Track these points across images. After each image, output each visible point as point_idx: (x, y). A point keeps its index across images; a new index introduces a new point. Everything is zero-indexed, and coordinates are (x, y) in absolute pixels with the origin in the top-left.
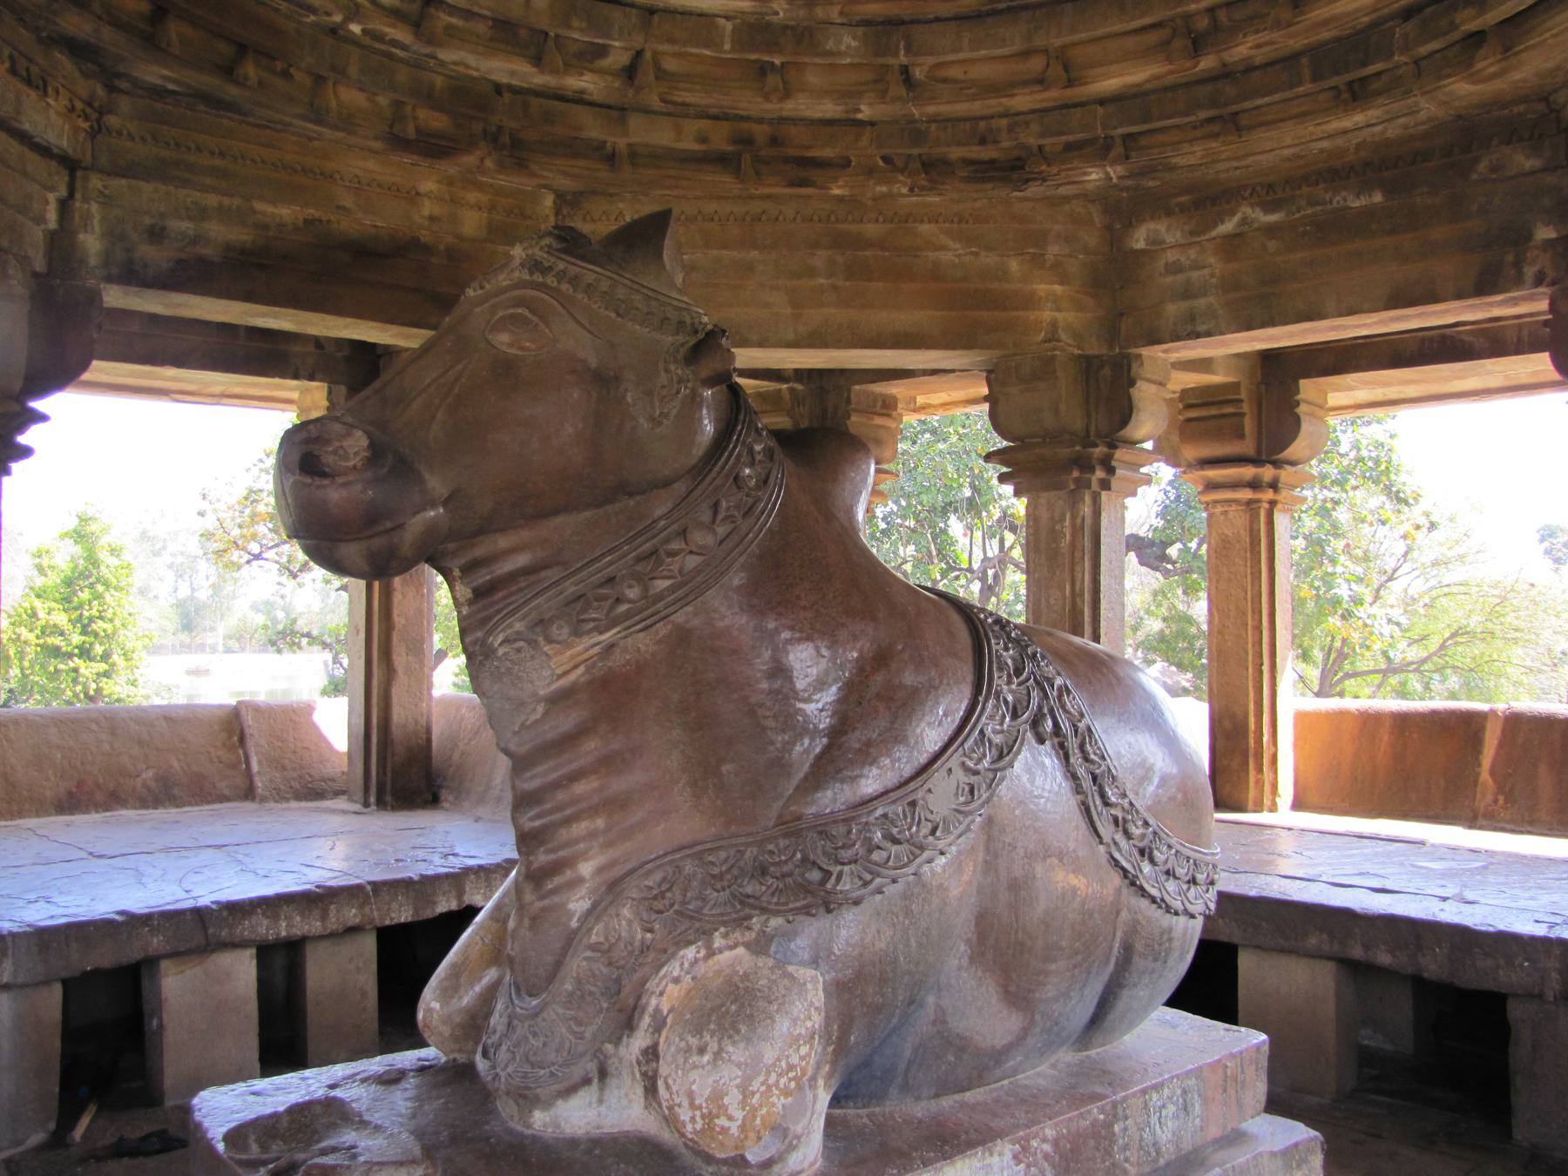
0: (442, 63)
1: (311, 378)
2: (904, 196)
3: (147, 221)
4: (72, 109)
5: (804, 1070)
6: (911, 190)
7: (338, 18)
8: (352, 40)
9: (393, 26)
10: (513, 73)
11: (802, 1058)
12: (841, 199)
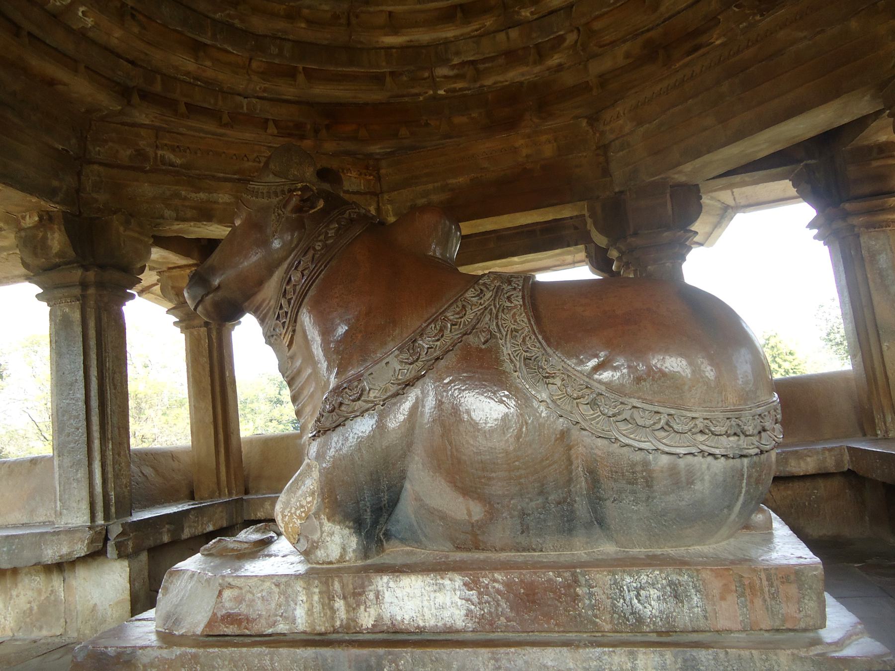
0: (489, 86)
1: (576, 244)
2: (760, 21)
3: (409, 204)
4: (361, 174)
5: (309, 510)
6: (762, 15)
7: (431, 92)
8: (442, 97)
9: (455, 83)
10: (523, 75)
11: (308, 503)
12: (722, 44)
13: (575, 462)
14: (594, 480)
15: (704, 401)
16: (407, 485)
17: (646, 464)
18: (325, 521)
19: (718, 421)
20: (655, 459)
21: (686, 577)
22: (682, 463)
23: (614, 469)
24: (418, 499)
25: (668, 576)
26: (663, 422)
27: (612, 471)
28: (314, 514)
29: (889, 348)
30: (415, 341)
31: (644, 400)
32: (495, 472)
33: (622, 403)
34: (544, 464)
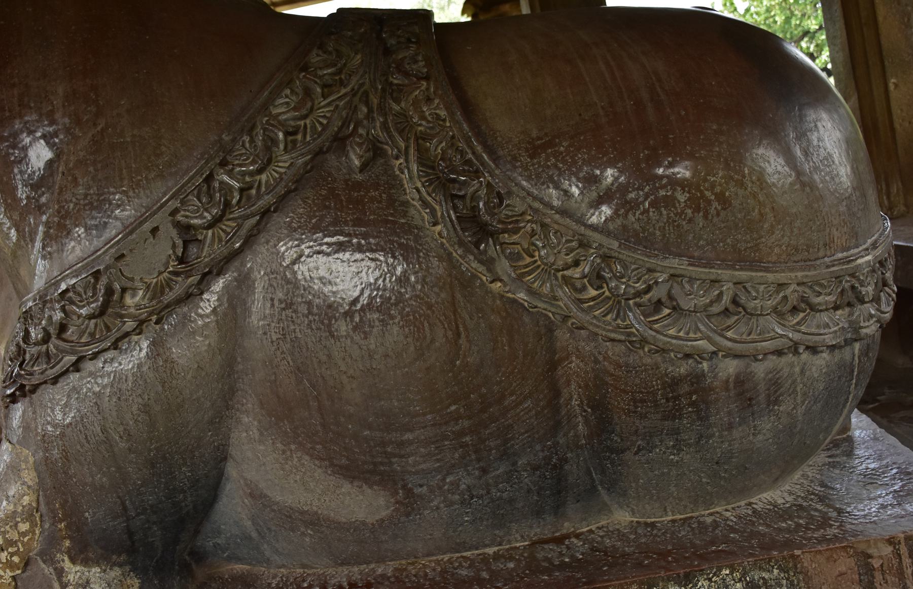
11: (24, 534)
13: (565, 393)
14: (598, 406)
15: (797, 250)
16: (231, 470)
17: (697, 378)
18: (67, 564)
19: (821, 285)
20: (712, 369)
21: (776, 571)
22: (760, 369)
23: (639, 396)
24: (256, 495)
25: (744, 575)
26: (726, 299)
27: (635, 401)
28: (42, 554)
29: (896, 85)
30: (209, 179)
31: (695, 261)
32: (411, 431)
33: (650, 270)
34: (506, 403)
